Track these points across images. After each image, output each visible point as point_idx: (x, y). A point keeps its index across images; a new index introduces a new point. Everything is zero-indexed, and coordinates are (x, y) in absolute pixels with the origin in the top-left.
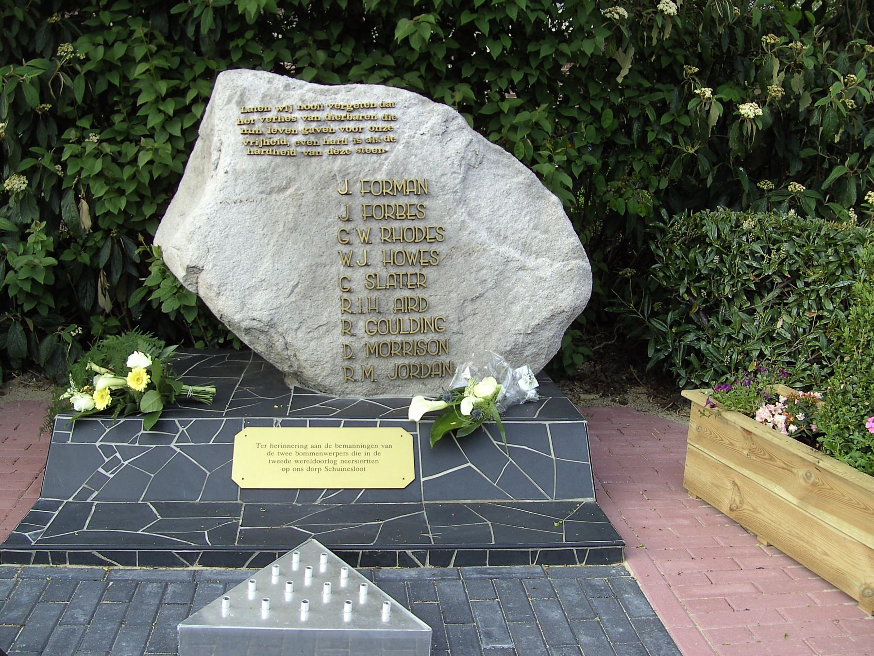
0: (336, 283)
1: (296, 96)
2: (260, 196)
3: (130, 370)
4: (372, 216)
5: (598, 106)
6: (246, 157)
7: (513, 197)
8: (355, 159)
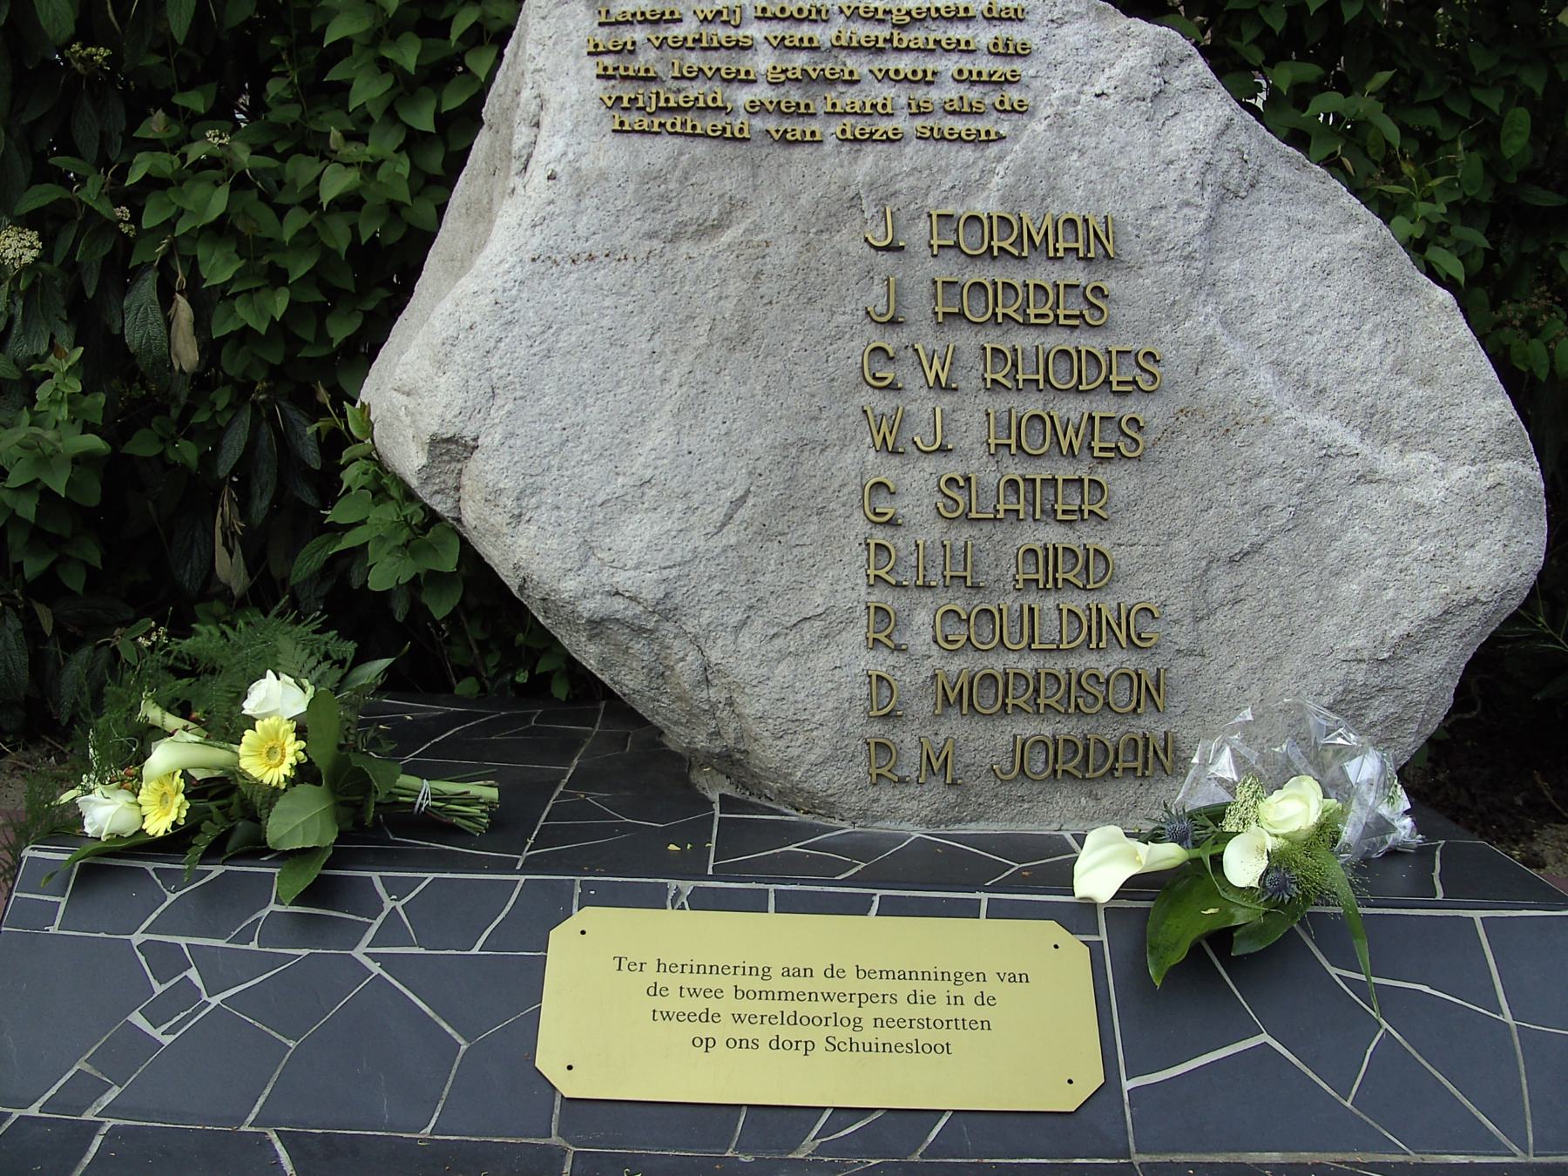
0: (856, 498)
2: (647, 245)
3: (251, 722)
4: (961, 314)
5: (1493, 100)
6: (609, 137)
7: (1341, 282)
8: (913, 154)
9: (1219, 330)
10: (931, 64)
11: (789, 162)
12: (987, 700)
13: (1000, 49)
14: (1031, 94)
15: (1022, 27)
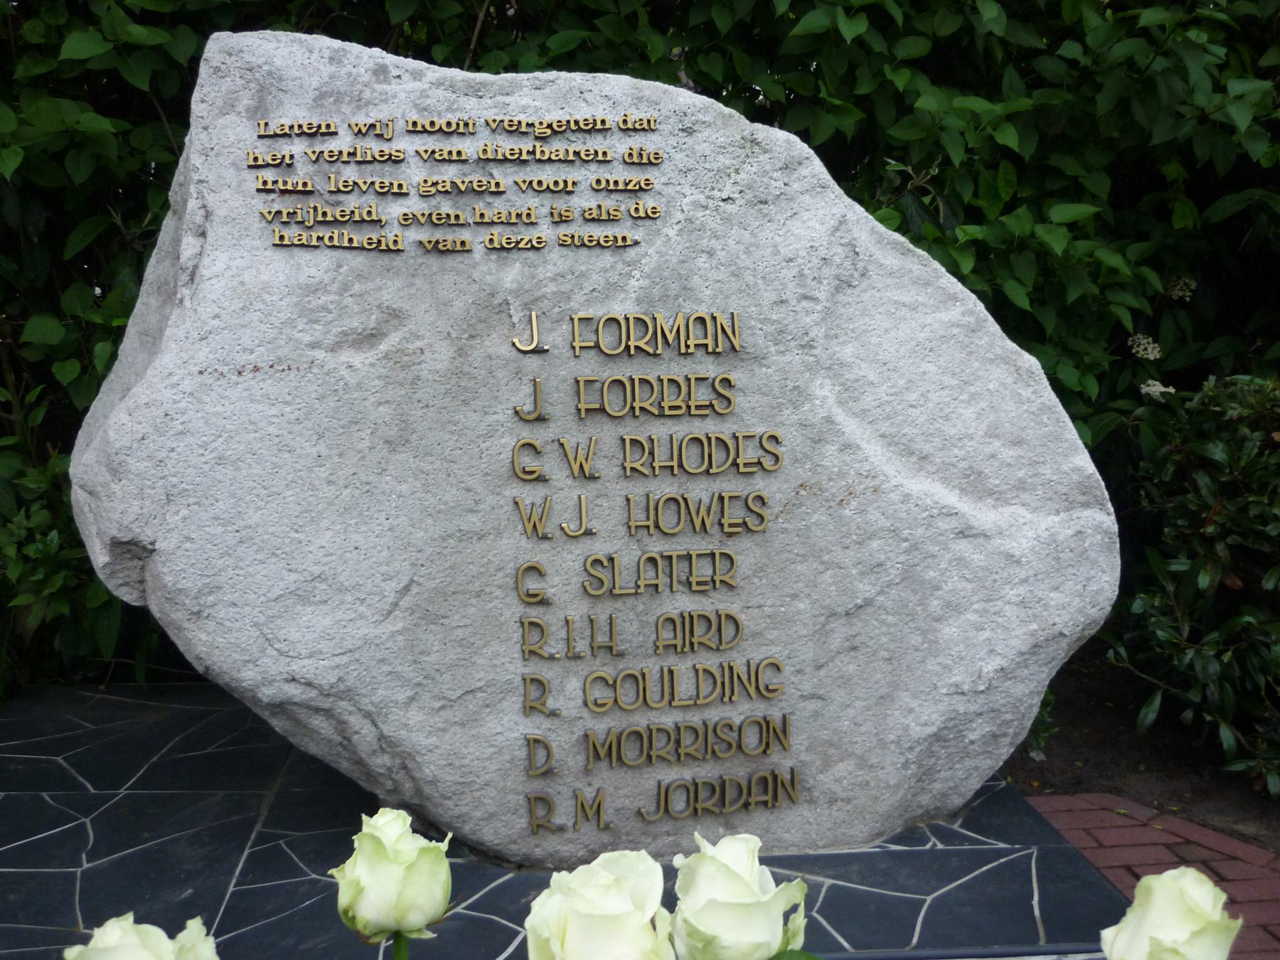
1: (402, 96)
4: (602, 410)
13: (635, 160)
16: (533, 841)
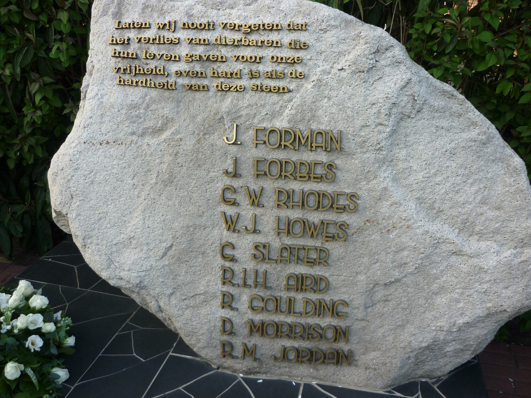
8: (250, 98)
9: (390, 184)
10: (260, 53)
11: (194, 99)
12: (271, 331)
14: (307, 68)
15: (305, 34)
16: (223, 360)
